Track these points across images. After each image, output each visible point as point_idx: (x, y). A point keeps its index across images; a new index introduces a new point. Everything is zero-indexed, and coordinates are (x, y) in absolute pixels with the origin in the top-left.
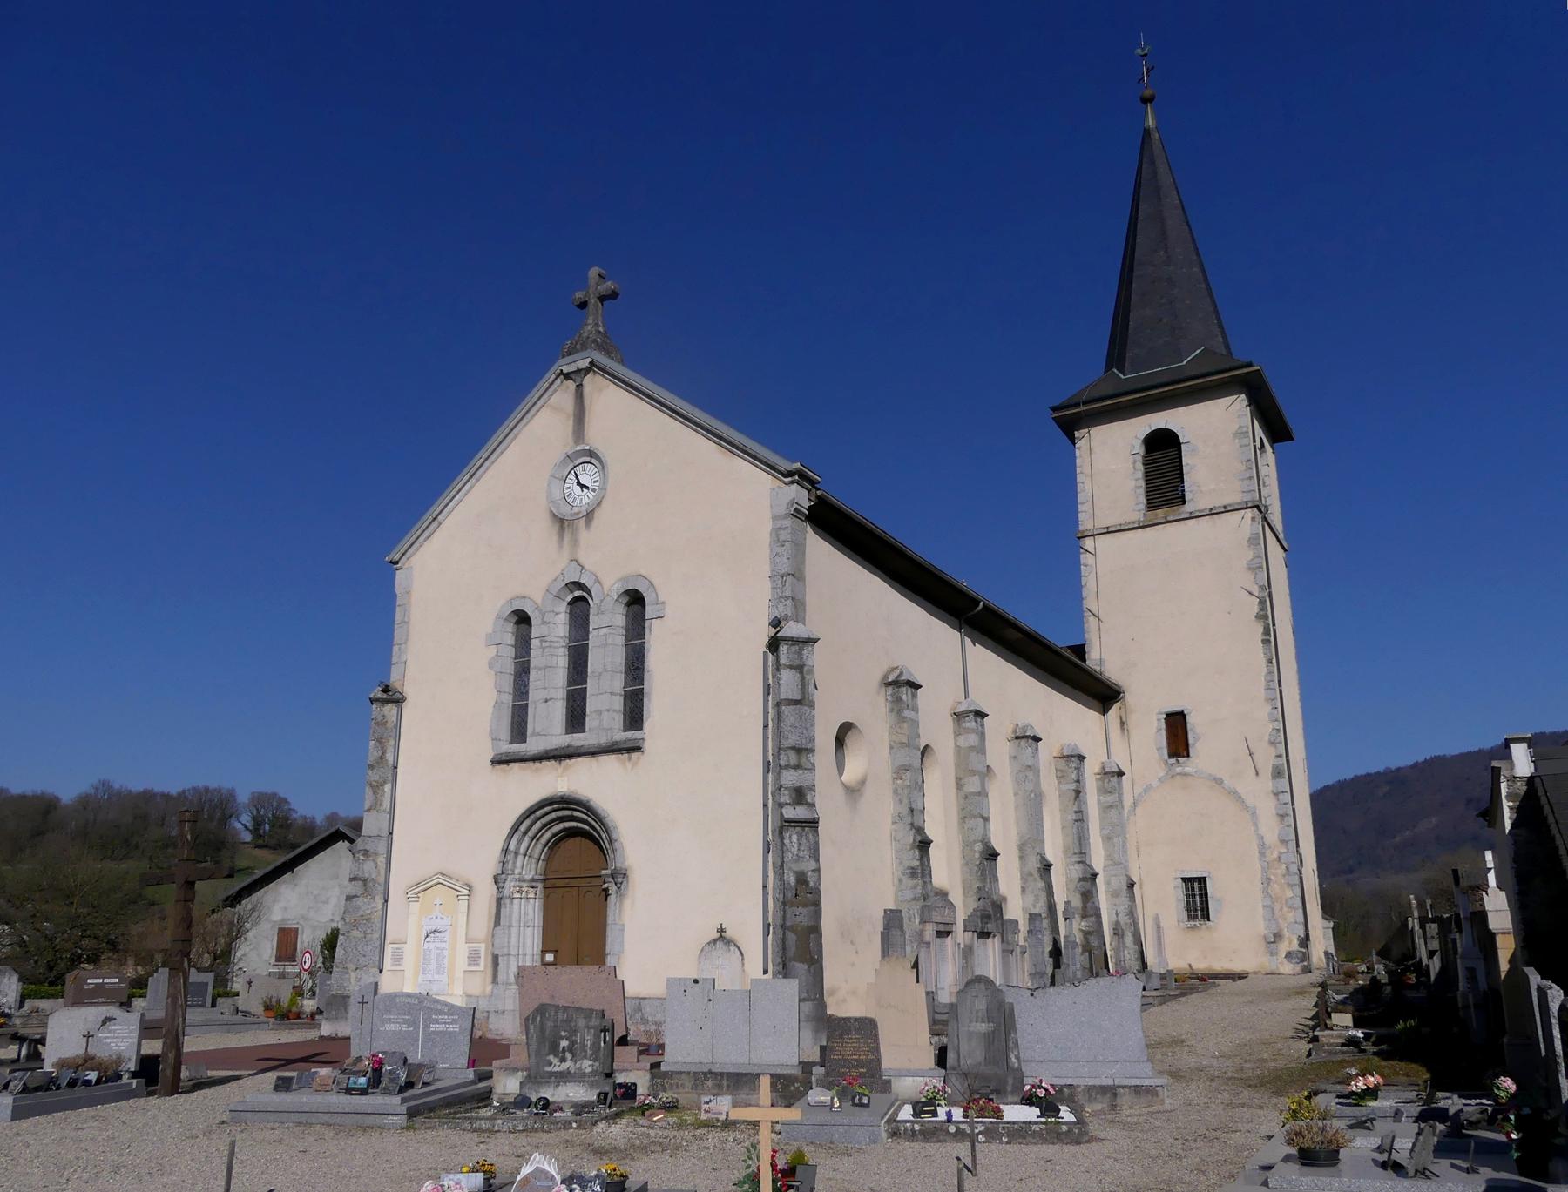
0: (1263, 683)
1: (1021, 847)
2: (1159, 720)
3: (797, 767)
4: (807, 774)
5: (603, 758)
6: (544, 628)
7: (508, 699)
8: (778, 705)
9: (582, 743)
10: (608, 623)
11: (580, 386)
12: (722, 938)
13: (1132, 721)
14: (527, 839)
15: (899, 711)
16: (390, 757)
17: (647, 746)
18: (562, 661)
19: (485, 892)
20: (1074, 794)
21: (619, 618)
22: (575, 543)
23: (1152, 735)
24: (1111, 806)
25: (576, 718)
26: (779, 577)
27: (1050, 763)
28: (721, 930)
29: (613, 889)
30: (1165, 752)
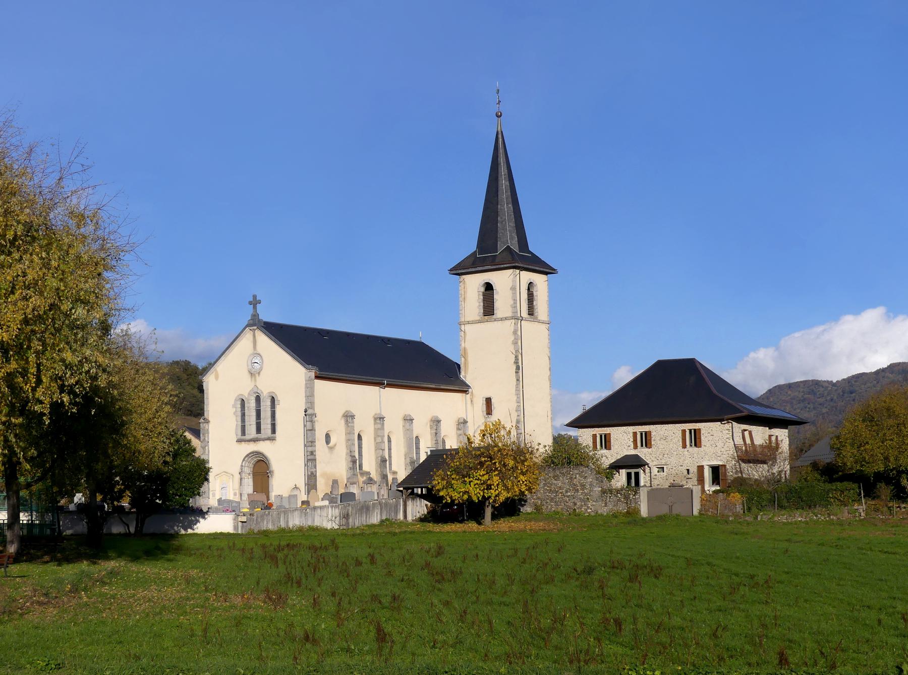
0: (515, 388)
1: (405, 455)
2: (483, 400)
3: (311, 446)
4: (314, 448)
5: (266, 441)
6: (248, 404)
7: (240, 423)
8: (307, 431)
9: (260, 437)
10: (266, 405)
11: (254, 333)
12: (296, 488)
13: (475, 400)
14: (250, 459)
15: (348, 424)
16: (207, 439)
17: (277, 438)
18: (254, 414)
19: (237, 477)
20: (435, 434)
21: (269, 403)
22: (255, 380)
23: (480, 405)
24: (460, 435)
25: (259, 430)
26: (307, 397)
27: (427, 424)
28: (296, 485)
29: (270, 476)
30: (485, 413)
